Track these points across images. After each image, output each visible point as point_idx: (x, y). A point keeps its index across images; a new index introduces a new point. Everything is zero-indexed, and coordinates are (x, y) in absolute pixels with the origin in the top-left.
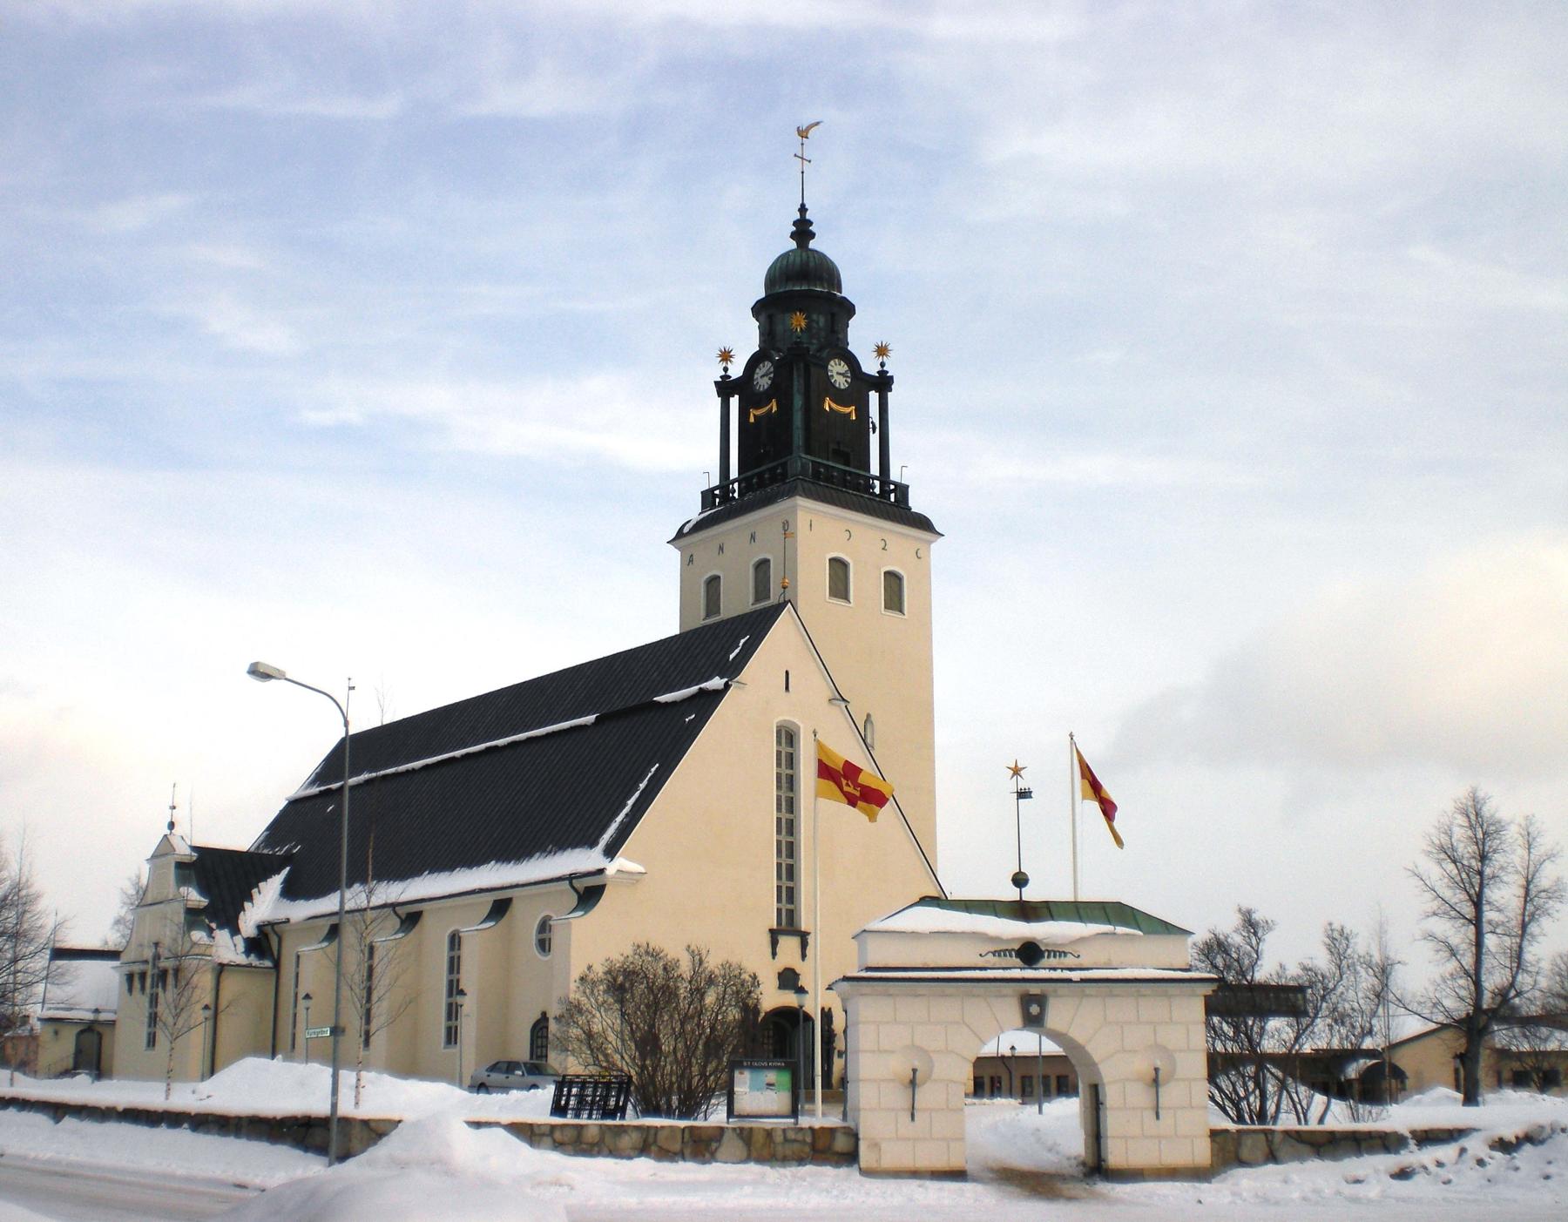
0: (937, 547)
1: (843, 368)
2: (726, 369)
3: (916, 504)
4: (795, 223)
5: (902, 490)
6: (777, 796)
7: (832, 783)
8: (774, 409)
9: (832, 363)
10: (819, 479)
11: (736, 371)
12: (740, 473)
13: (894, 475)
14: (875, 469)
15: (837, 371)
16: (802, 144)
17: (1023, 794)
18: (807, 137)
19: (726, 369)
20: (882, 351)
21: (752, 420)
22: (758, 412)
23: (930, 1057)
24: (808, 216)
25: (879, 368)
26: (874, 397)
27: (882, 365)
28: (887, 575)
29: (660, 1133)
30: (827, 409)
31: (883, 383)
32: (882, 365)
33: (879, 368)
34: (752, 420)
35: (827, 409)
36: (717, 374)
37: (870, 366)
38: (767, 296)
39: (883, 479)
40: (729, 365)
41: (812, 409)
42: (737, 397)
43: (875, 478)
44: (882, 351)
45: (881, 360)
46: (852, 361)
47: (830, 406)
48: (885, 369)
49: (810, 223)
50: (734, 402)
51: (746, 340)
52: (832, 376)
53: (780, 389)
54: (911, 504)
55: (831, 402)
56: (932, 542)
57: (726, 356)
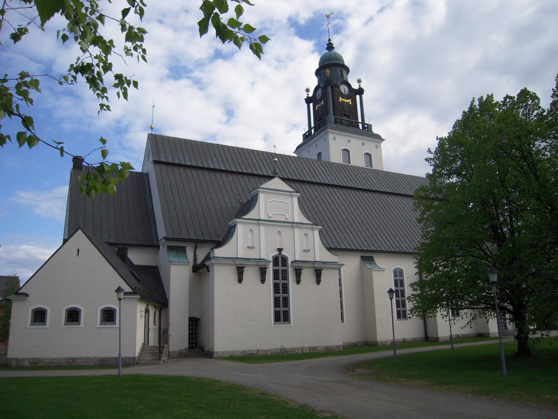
0: (383, 144)
1: (346, 87)
2: (308, 95)
3: (375, 130)
4: (328, 45)
5: (369, 126)
6: (397, 311)
7: (295, 150)
8: (323, 103)
9: (341, 86)
10: (337, 123)
11: (311, 94)
12: (314, 124)
13: (367, 122)
14: (360, 120)
15: (344, 89)
16: (328, 20)
17: (462, 328)
18: (329, 18)
19: (308, 95)
20: (359, 81)
21: (317, 109)
22: (318, 106)
23: (253, 197)
24: (331, 42)
25: (359, 87)
26: (358, 97)
27: (360, 86)
28: (365, 155)
29: (259, 351)
30: (341, 101)
31: (360, 91)
32: (360, 86)
33: (359, 87)
34: (317, 109)
35: (341, 101)
36: (305, 97)
37: (355, 86)
38: (319, 67)
39: (363, 123)
40: (309, 93)
41: (335, 101)
42: (312, 103)
43: (360, 123)
44: (359, 81)
45: (359, 84)
46: (349, 86)
47: (342, 100)
48: (361, 87)
49: (332, 44)
50: (311, 105)
51: (313, 82)
52: (342, 90)
53: (324, 96)
54: (373, 130)
55: (342, 99)
56: (382, 142)
57: (308, 90)
